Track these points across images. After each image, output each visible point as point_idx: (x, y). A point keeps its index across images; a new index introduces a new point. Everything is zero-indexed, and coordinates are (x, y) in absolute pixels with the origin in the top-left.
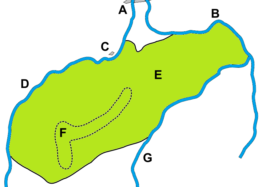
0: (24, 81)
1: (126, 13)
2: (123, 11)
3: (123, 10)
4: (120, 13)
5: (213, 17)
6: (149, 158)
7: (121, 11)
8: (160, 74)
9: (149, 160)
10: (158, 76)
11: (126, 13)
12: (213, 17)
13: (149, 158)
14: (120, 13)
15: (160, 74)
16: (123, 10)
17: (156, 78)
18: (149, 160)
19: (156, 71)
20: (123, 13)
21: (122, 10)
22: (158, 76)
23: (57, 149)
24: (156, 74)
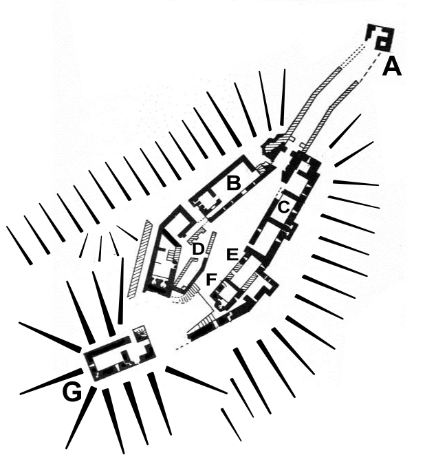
0: (187, 223)
1: (399, 73)
2: (392, 69)
3: (392, 66)
4: (385, 73)
5: (229, 188)
6: (74, 392)
7: (387, 69)
8: (236, 254)
9: (75, 396)
10: (232, 257)
11: (399, 73)
12: (229, 188)
13: (74, 392)
14: (385, 73)
15: (236, 254)
16: (392, 66)
17: (229, 259)
18: (75, 396)
19: (229, 250)
20: (392, 74)
21: (393, 67)
22: (232, 257)
23: (180, 349)
24: (229, 254)
